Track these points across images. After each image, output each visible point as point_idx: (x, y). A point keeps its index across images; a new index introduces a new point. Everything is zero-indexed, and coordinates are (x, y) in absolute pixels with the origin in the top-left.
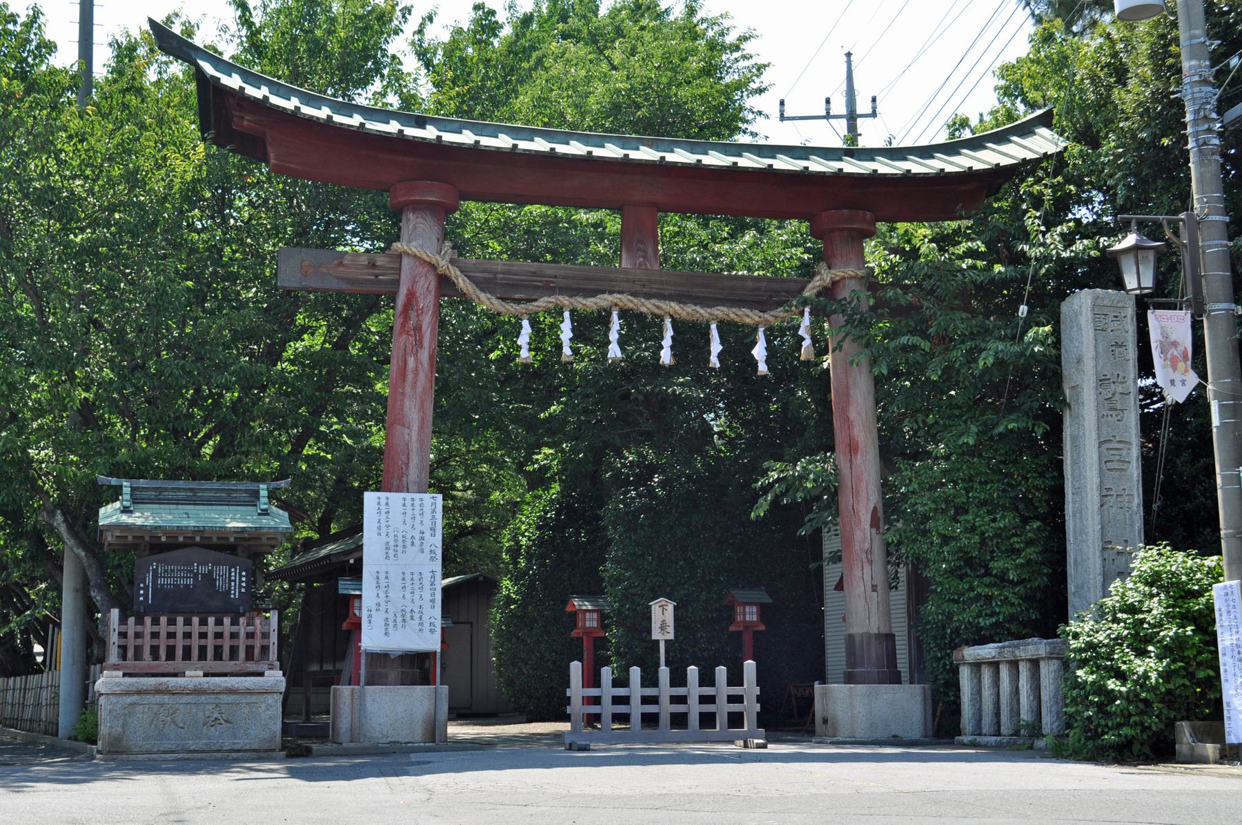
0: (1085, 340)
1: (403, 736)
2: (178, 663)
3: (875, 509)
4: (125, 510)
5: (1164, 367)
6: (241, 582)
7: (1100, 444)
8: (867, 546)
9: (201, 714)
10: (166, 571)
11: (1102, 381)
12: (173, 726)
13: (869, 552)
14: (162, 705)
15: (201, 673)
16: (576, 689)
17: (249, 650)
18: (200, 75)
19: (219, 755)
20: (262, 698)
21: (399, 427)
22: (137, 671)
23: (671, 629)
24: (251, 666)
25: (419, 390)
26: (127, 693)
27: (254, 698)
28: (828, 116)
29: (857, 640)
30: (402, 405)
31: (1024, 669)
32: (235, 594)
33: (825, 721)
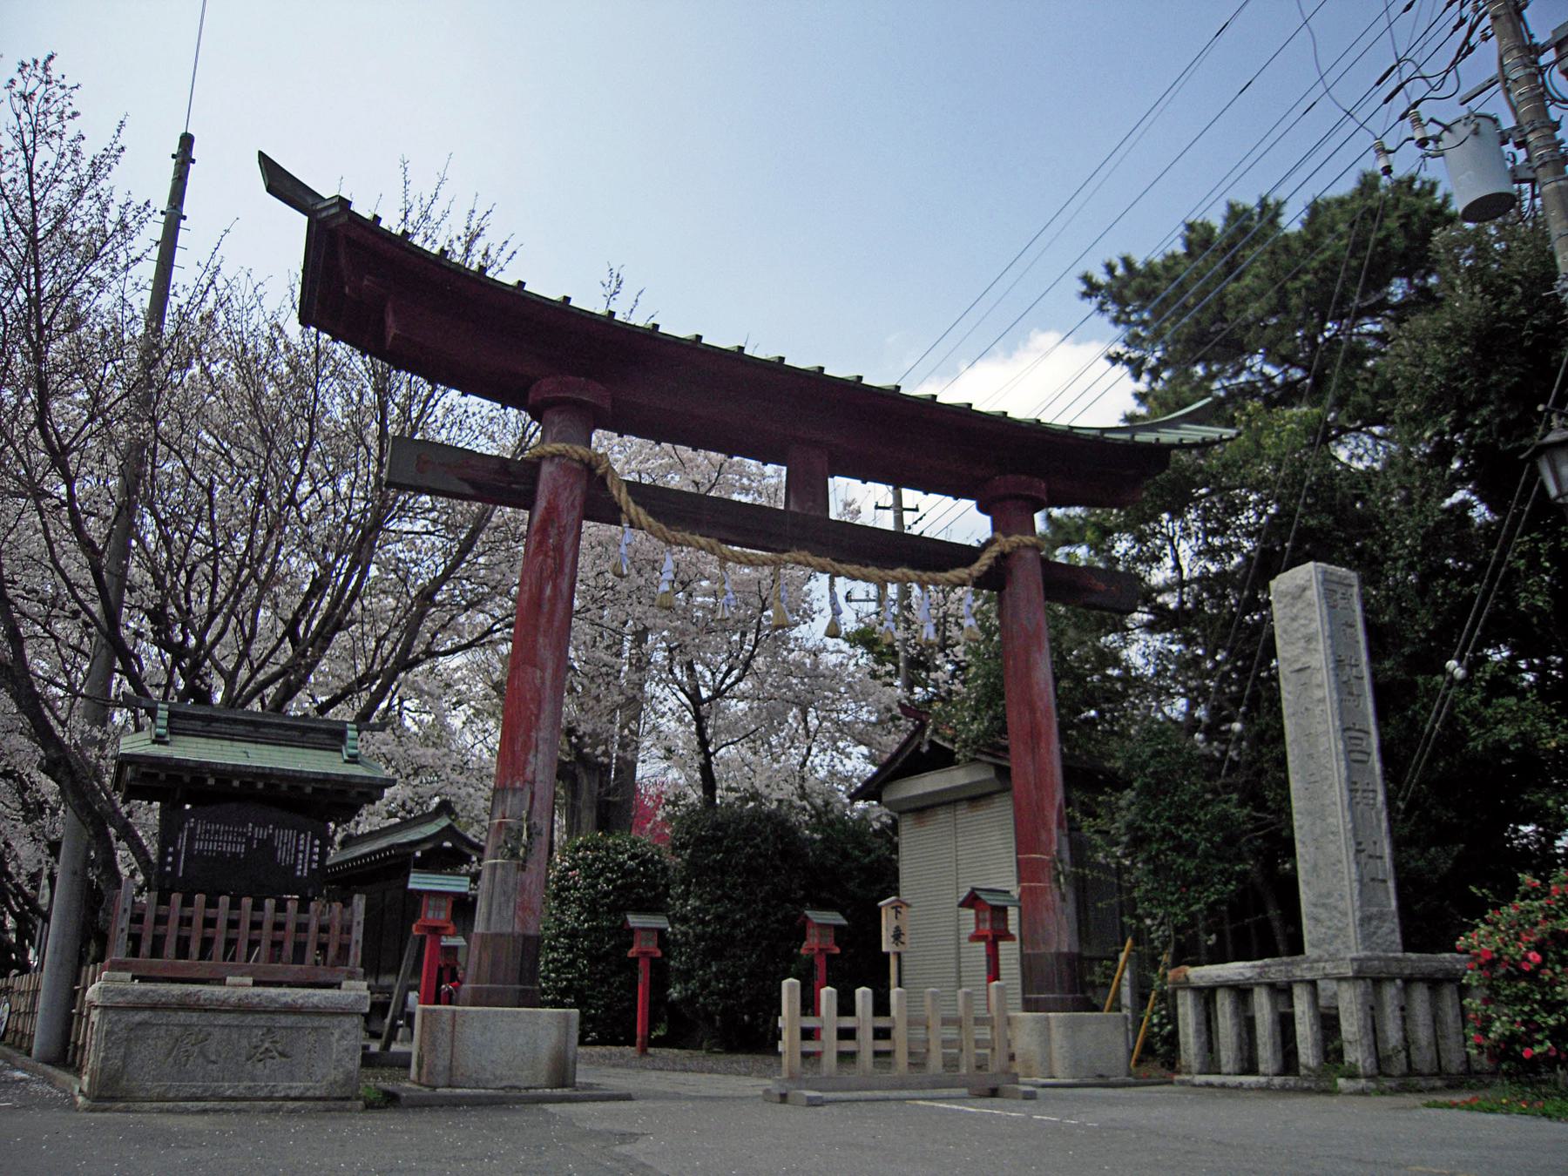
1: (524, 1077)
2: (216, 962)
6: (312, 853)
9: (244, 1042)
10: (207, 831)
12: (201, 1060)
14: (186, 1026)
15: (249, 980)
16: (789, 1017)
19: (268, 1104)
20: (335, 1021)
21: (530, 670)
22: (154, 974)
24: (323, 974)
25: (556, 624)
27: (324, 1021)
30: (535, 641)
32: (302, 871)
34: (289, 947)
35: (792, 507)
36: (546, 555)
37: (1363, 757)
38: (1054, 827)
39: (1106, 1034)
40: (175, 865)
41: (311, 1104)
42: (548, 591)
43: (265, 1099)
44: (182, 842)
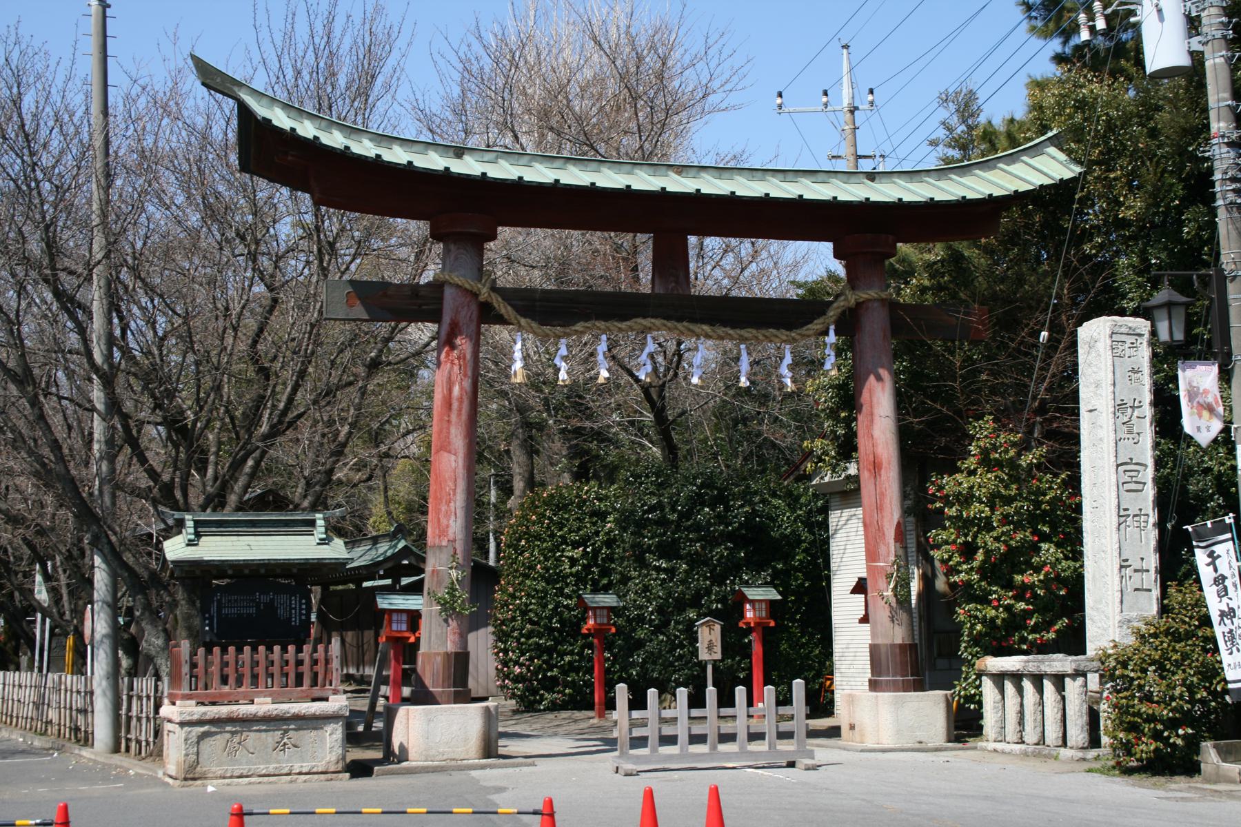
5: (1191, 414)
6: (301, 609)
7: (1118, 466)
11: (1120, 406)
18: (245, 113)
21: (446, 454)
23: (718, 649)
26: (200, 723)
29: (883, 650)
30: (449, 433)
33: (852, 727)
34: (292, 676)
35: (657, 291)
36: (452, 363)
37: (1139, 487)
38: (892, 542)
39: (928, 710)
41: (316, 776)
44: (214, 610)
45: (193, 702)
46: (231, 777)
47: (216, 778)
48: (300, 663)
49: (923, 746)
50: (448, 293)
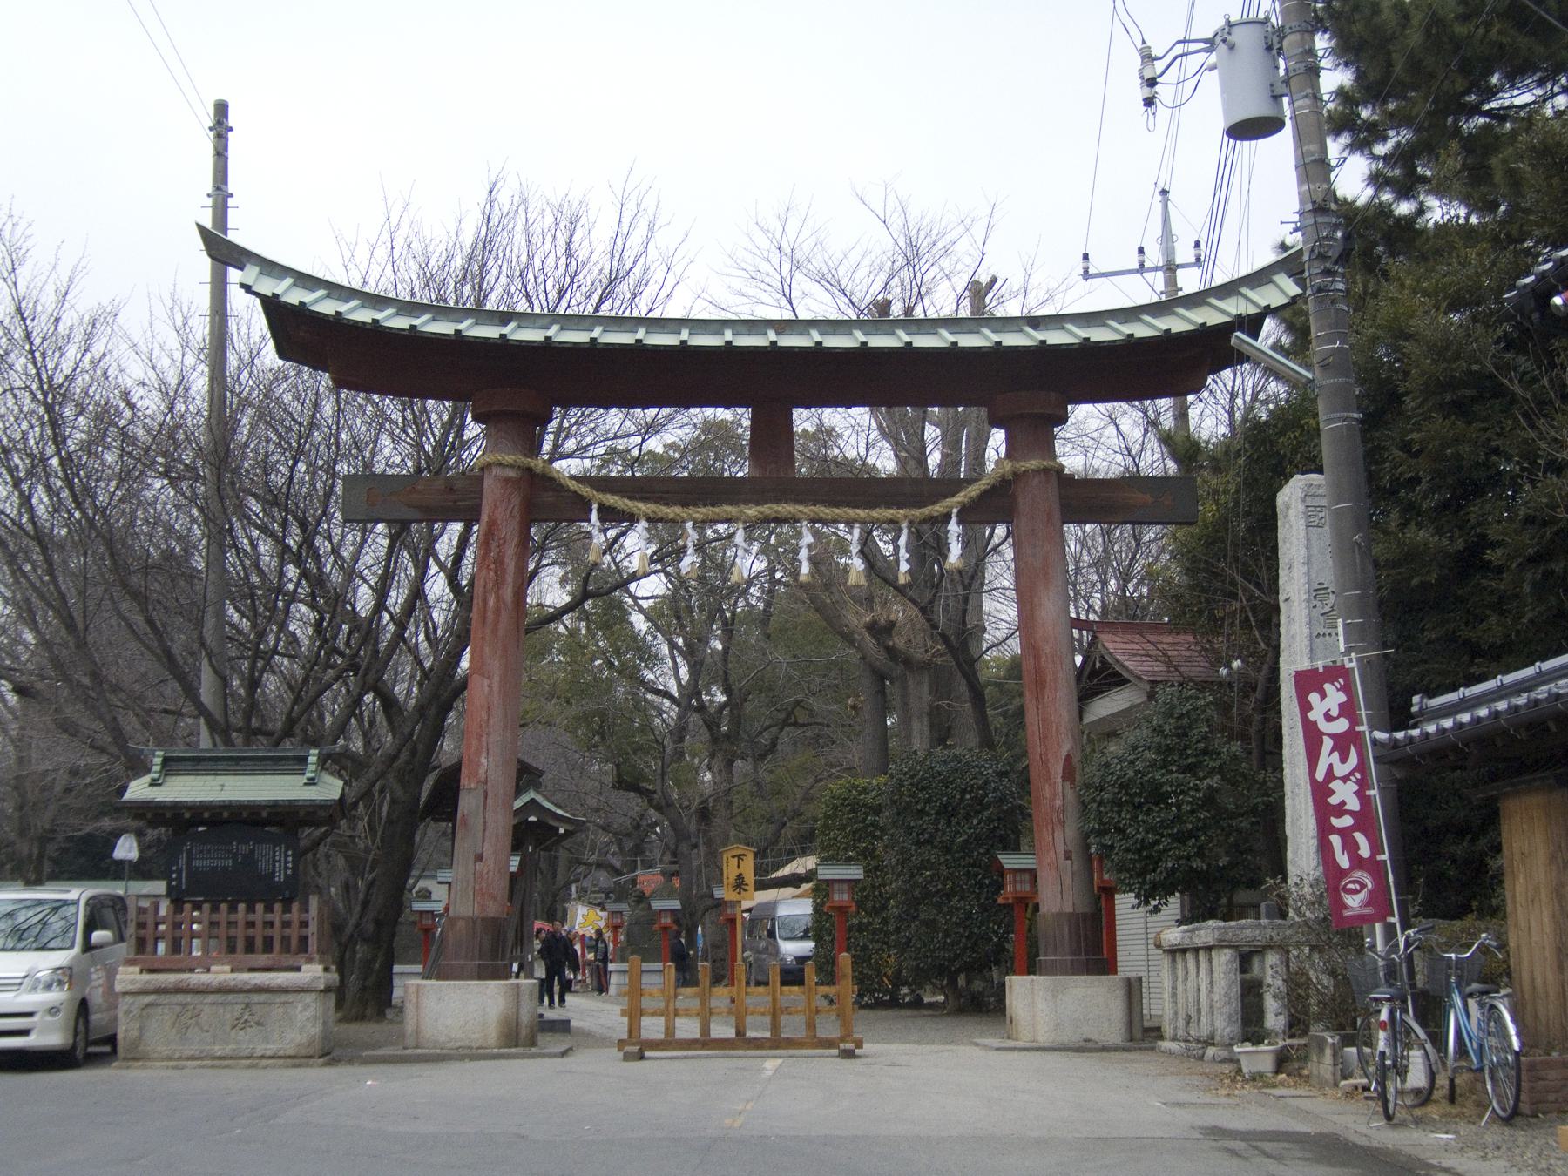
0: (1294, 539)
3: (1068, 757)
4: (154, 783)
6: (286, 862)
8: (1058, 803)
13: (1063, 809)
15: (227, 968)
17: (285, 940)
25: (501, 633)
26: (143, 992)
27: (290, 997)
28: (1142, 268)
31: (91, 1049)
32: (280, 877)
40: (179, 879)
42: (492, 602)
43: (248, 1058)
45: (137, 969)
46: (180, 1059)
47: (163, 1060)
48: (304, 924)
49: (1089, 1045)
50: (488, 482)
